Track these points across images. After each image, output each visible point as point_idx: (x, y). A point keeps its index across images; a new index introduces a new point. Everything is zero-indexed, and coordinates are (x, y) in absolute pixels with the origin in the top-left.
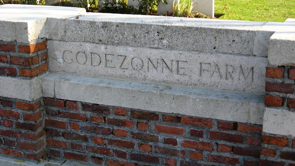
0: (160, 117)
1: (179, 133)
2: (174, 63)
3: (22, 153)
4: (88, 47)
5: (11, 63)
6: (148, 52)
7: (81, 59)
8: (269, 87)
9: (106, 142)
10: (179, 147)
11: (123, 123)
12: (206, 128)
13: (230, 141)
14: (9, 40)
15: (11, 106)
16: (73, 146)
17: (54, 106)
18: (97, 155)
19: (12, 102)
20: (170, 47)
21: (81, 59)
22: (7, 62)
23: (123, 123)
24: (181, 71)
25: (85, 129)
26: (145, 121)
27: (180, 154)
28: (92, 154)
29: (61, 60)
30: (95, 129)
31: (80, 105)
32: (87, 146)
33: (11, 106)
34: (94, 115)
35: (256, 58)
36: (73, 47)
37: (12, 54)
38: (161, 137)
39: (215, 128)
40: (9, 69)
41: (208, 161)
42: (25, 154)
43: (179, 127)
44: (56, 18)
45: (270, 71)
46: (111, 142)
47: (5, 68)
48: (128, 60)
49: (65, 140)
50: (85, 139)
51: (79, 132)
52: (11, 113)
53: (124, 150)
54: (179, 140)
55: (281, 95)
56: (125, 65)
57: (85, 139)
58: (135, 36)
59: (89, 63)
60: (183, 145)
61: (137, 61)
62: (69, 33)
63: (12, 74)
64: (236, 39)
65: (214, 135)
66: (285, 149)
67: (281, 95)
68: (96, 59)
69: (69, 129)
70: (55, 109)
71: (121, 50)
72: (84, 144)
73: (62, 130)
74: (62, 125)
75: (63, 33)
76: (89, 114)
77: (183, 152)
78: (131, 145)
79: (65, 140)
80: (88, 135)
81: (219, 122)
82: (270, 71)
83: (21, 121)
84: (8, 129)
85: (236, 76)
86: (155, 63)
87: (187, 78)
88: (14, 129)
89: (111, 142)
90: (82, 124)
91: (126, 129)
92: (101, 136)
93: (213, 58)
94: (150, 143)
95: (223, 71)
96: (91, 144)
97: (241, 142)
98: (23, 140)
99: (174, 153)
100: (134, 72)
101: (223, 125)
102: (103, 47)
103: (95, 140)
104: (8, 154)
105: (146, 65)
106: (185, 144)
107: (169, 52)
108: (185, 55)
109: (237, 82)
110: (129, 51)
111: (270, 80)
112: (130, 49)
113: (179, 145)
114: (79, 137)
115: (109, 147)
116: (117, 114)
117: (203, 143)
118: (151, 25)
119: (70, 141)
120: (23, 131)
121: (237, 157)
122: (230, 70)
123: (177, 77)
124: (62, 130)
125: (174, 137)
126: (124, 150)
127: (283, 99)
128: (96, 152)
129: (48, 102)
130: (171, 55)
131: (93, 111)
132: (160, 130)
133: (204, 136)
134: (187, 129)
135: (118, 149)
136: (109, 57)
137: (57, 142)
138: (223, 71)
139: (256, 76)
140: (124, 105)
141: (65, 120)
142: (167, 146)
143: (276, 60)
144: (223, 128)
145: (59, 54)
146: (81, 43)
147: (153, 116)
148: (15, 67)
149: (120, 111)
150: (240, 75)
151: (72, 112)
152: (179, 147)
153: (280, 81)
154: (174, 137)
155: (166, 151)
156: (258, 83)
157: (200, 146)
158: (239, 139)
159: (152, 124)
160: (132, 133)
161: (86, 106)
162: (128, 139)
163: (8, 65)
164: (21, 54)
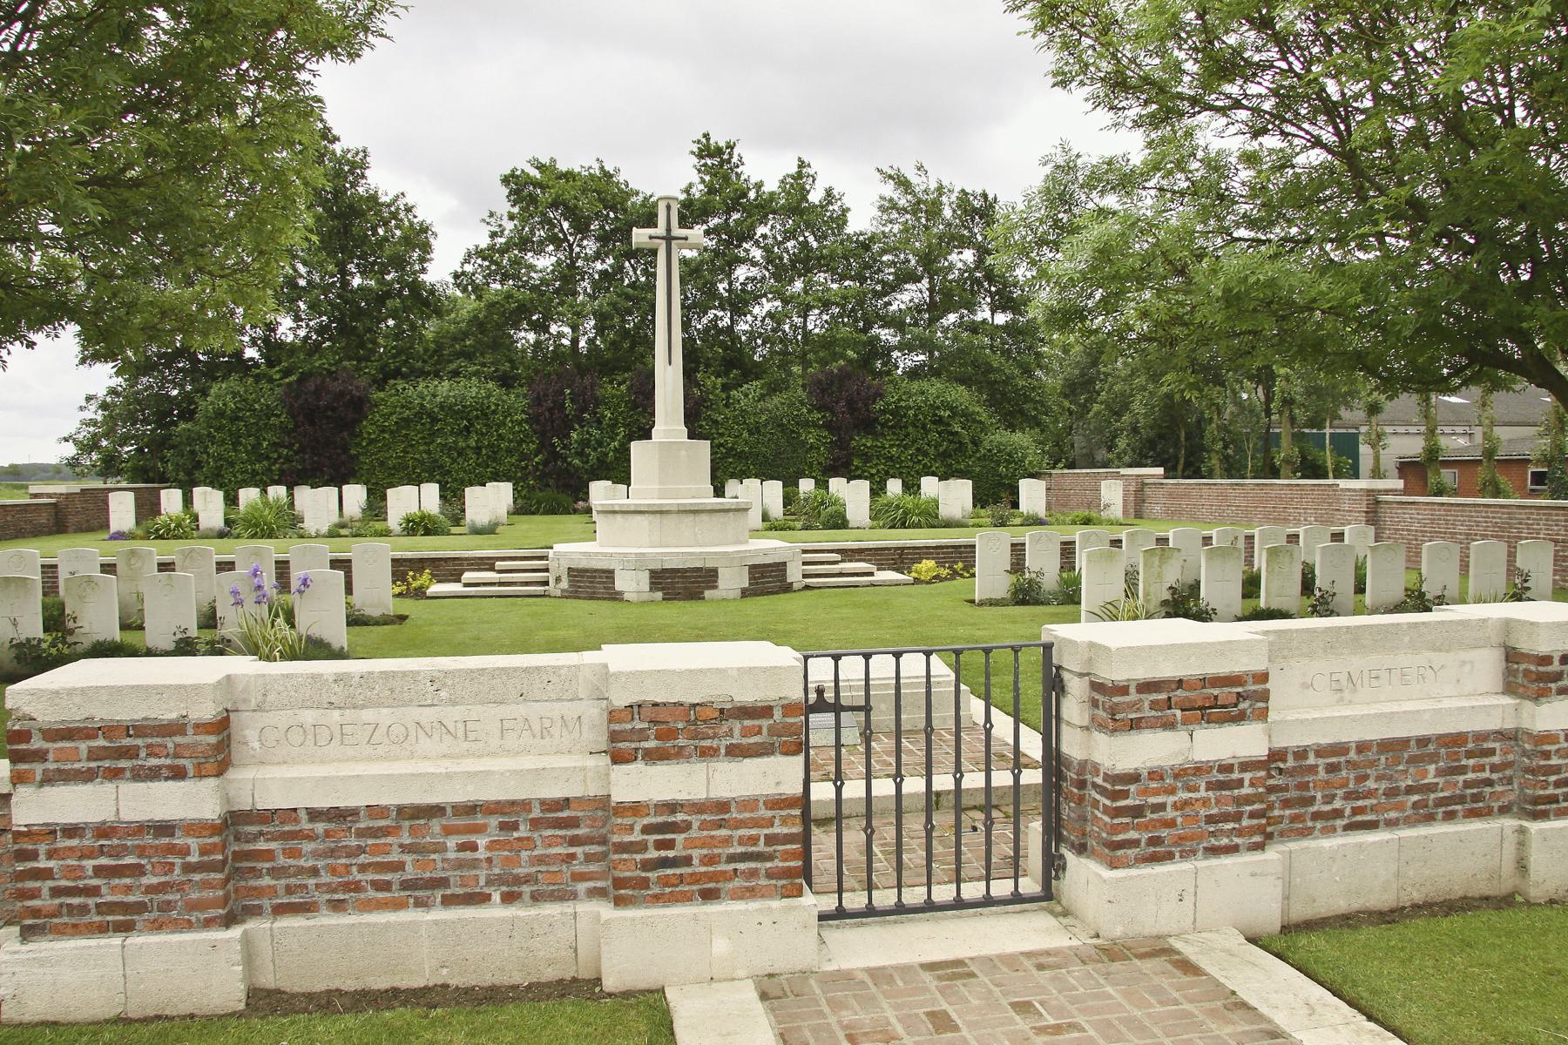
0: (449, 810)
1: (479, 829)
2: (461, 725)
3: (193, 919)
4: (309, 717)
5: (176, 756)
6: (415, 713)
7: (296, 736)
8: (614, 737)
9: (354, 869)
10: (482, 854)
12: (524, 815)
13: (561, 828)
14: (174, 716)
15: (172, 835)
16: (289, 890)
17: (251, 824)
18: (336, 897)
19: (174, 827)
20: (453, 702)
21: (296, 736)
22: (167, 756)
23: (386, 832)
24: (472, 736)
25: (316, 854)
26: (422, 822)
27: (485, 865)
28: (328, 897)
29: (256, 745)
30: (332, 851)
31: (303, 815)
32: (317, 885)
33: (172, 835)
34: (332, 826)
35: (585, 702)
36: (282, 719)
37: (178, 739)
38: (452, 842)
40: (169, 767)
42: (198, 920)
43: (480, 819)
45: (613, 715)
46: (363, 868)
47: (160, 767)
48: (382, 729)
49: (273, 882)
50: (314, 872)
51: (302, 862)
52: (171, 850)
53: (388, 877)
54: (482, 841)
55: (633, 745)
56: (375, 740)
57: (314, 872)
58: (392, 691)
59: (310, 741)
60: (489, 848)
61: (397, 730)
62: (271, 697)
63: (178, 774)
64: (554, 679)
65: (536, 824)
66: (646, 821)
67: (633, 745)
68: (324, 734)
69: (282, 861)
70: (253, 829)
71: (368, 715)
72: (312, 882)
73: (267, 865)
74: (269, 855)
75: (260, 698)
76: (320, 827)
77: (489, 860)
78: (400, 866)
79: (273, 882)
80: (320, 864)
81: (543, 802)
82: (613, 715)
83: (194, 858)
84: (163, 879)
85: (556, 731)
86: (428, 729)
87: (480, 745)
88: (177, 875)
89: (363, 868)
90: (308, 847)
91: (389, 840)
92: (343, 861)
93: (521, 710)
94: (433, 856)
95: (536, 727)
96: (325, 878)
97: (578, 826)
98: (194, 896)
99: (474, 864)
100: (393, 747)
102: (336, 713)
103: (333, 871)
104: (160, 928)
105: (413, 733)
106: (490, 847)
107: (450, 708)
108: (476, 711)
110: (384, 715)
111: (617, 727)
112: (385, 711)
113: (481, 849)
114: (301, 871)
115: (359, 877)
116: (372, 817)
117: (519, 839)
118: (418, 672)
119: (283, 882)
120: (197, 877)
121: (572, 850)
122: (547, 724)
123: (466, 745)
124: (267, 865)
125: (473, 838)
126: (388, 877)
127: (636, 749)
128: (335, 891)
130: (452, 715)
131: (330, 820)
132: (448, 831)
133: (522, 827)
135: (377, 877)
136: (347, 729)
137: (255, 888)
138: (536, 727)
139: (585, 728)
140: (384, 802)
141: (273, 845)
142: (461, 855)
144: (550, 810)
145: (251, 735)
147: (436, 811)
148: (181, 762)
149: (375, 811)
151: (287, 828)
153: (629, 726)
154: (473, 838)
155: (460, 865)
157: (516, 845)
158: (573, 823)
159: (436, 825)
160: (401, 846)
162: (395, 857)
163: (168, 762)
164: (198, 738)
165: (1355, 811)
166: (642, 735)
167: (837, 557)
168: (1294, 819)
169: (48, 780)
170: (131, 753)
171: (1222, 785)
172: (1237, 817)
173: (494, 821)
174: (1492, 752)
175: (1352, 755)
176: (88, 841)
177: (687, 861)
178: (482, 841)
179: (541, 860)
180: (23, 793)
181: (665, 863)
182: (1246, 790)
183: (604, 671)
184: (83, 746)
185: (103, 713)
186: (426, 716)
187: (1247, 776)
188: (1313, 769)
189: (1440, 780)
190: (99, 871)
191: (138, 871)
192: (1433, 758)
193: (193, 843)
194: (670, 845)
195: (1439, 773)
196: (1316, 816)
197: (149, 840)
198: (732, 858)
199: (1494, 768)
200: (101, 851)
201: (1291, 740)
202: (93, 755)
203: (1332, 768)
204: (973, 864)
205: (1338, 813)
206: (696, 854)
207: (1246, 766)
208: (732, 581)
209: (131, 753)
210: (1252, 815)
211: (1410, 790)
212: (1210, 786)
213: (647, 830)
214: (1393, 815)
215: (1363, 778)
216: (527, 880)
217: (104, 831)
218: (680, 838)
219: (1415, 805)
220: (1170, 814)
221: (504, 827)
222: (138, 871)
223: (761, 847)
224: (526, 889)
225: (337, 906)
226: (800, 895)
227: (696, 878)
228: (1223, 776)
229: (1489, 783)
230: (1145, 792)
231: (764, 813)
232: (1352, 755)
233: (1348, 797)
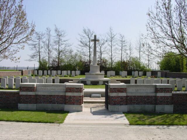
4: (42, 88)
8: (66, 90)
11: (48, 97)
21: (41, 89)
23: (48, 97)
38: (53, 98)
39: (60, 96)
41: (54, 61)
44: (90, 70)
45: (66, 88)
46: (46, 100)
52: (31, 97)
54: (55, 98)
57: (42, 100)
65: (60, 97)
69: (40, 99)
71: (47, 88)
76: (43, 96)
78: (49, 100)
82: (66, 88)
83: (33, 98)
90: (41, 98)
99: (55, 100)
101: (61, 96)
106: (56, 99)
109: (62, 90)
110: (48, 88)
129: (36, 95)
134: (56, 97)
143: (67, 87)
146: (150, 22)
147: (52, 96)
150: (25, 38)
152: (55, 99)
155: (54, 100)
156: (65, 90)
159: (52, 97)
161: (42, 95)
165: (137, 102)
166: (68, 90)
167: (116, 81)
168: (130, 103)
169: (22, 91)
170: (28, 89)
171: (121, 98)
172: (123, 101)
173: (56, 97)
174: (153, 98)
175: (137, 97)
176: (25, 96)
177: (72, 101)
178: (55, 98)
179: (60, 100)
180: (20, 92)
181: (70, 101)
182: (124, 99)
183: (66, 85)
184: (25, 89)
185: (26, 86)
186: (52, 88)
187: (124, 98)
188: (132, 98)
189: (147, 100)
190: (26, 99)
191: (28, 99)
192: (146, 98)
193: (33, 97)
194: (70, 99)
195: (147, 99)
196: (133, 103)
197: (29, 96)
198: (76, 101)
199: (153, 99)
200: (26, 97)
201: (129, 95)
202: (26, 89)
203: (134, 98)
204: (81, 98)
205: (135, 102)
206: (72, 100)
207: (124, 97)
208: (101, 83)
209: (28, 89)
210: (125, 101)
211: (143, 101)
212: (120, 98)
213: (69, 98)
214: (141, 103)
215: (138, 99)
216: (59, 102)
217: (26, 95)
218: (71, 99)
219: (144, 103)
220: (116, 100)
221: (57, 97)
222: (28, 99)
223: (78, 100)
224: (59, 103)
225: (44, 103)
226: (82, 106)
227: (73, 102)
228: (121, 98)
229: (152, 101)
230: (113, 98)
231: (78, 97)
232: (137, 97)
233: (136, 101)
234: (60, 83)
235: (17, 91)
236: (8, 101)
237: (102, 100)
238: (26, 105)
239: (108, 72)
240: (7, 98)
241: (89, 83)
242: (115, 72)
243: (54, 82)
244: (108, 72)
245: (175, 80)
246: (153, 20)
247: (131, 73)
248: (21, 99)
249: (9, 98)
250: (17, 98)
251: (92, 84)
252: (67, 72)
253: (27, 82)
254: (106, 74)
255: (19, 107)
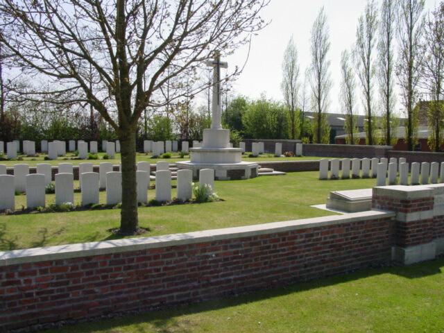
209: (422, 205)
217: (418, 222)
234: (30, 173)
235: (382, 215)
236: (370, 244)
237: (277, 210)
238: (418, 247)
239: (24, 142)
240: (366, 236)
241: (224, 174)
242: (36, 144)
243: (76, 171)
244: (24, 142)
245: (330, 163)
246: (194, 21)
247: (274, 146)
248: (409, 232)
249: (370, 235)
250: (387, 233)
251: (229, 178)
252: (165, 145)
253: (385, 185)
254: (249, 148)
255: (406, 258)
